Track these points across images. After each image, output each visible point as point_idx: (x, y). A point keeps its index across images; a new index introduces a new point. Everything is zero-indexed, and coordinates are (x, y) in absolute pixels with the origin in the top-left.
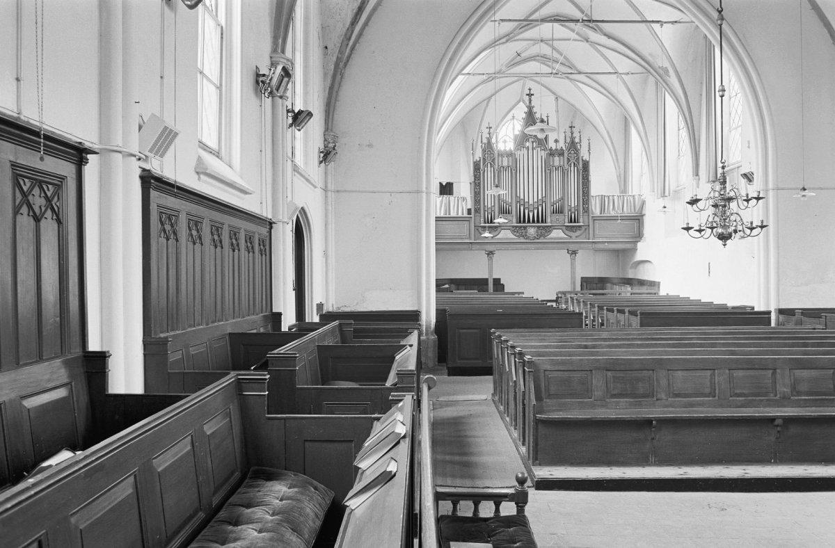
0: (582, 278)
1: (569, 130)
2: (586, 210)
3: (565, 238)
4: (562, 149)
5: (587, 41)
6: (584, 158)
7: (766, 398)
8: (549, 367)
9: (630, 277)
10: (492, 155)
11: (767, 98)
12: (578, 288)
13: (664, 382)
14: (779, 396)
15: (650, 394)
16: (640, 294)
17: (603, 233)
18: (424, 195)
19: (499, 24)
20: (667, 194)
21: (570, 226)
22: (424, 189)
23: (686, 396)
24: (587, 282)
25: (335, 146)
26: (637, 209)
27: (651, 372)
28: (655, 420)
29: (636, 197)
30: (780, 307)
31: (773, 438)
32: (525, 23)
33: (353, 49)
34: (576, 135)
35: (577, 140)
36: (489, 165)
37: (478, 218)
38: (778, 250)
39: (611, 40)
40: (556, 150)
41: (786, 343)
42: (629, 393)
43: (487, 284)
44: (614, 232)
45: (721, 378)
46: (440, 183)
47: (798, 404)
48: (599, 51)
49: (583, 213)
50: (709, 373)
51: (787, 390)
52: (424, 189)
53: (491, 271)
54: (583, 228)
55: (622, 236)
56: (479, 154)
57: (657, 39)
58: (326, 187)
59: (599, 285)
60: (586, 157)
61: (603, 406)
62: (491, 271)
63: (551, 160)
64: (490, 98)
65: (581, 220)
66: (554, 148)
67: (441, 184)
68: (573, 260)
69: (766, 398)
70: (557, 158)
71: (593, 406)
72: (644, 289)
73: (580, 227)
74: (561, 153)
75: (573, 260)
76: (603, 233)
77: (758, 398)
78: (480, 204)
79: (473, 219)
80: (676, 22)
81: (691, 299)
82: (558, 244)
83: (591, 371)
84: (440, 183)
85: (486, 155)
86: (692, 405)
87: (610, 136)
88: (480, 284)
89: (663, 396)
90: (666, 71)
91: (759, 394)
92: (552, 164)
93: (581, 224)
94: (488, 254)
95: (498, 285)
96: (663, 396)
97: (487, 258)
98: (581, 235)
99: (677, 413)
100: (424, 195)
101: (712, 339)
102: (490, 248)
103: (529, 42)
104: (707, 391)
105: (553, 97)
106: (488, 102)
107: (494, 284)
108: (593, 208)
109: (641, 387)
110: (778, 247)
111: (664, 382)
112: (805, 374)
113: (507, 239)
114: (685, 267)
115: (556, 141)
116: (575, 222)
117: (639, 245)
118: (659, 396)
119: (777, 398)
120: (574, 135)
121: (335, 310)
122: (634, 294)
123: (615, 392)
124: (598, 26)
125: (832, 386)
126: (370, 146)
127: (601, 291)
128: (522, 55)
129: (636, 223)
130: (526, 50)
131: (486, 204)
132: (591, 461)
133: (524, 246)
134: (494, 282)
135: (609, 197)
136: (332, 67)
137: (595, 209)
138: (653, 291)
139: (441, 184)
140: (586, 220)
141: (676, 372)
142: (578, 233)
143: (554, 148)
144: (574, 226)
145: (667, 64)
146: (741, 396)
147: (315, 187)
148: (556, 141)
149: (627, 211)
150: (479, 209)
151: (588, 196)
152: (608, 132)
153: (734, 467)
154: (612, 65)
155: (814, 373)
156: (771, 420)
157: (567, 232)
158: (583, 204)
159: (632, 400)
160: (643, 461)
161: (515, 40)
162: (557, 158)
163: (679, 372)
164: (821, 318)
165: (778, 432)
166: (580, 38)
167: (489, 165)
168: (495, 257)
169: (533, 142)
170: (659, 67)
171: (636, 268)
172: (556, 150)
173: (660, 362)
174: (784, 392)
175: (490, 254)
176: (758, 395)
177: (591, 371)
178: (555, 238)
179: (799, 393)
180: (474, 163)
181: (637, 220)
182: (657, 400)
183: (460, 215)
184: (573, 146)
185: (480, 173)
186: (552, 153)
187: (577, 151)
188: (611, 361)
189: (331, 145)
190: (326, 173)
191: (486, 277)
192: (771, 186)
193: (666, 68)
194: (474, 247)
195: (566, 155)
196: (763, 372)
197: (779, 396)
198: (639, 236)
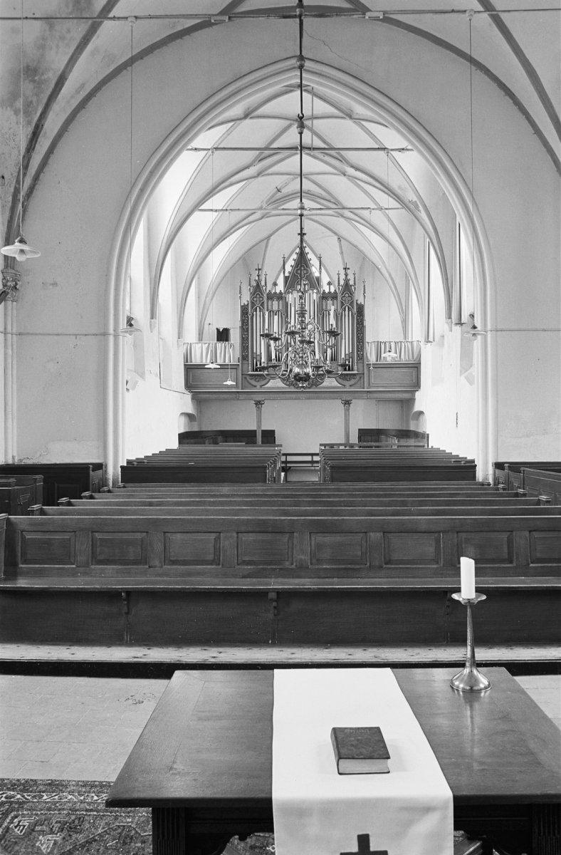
0: (359, 430)
1: (342, 272)
2: (361, 357)
3: (338, 387)
4: (281, 293)
5: (345, 175)
6: (359, 302)
7: (279, 567)
8: (27, 528)
9: (411, 429)
10: (261, 299)
11: (486, 236)
12: (354, 439)
13: (158, 547)
14: (295, 564)
15: (143, 560)
16: (407, 446)
17: (379, 381)
18: (111, 339)
19: (212, 152)
20: (431, 339)
21: (255, 375)
22: (111, 331)
23: (185, 563)
24: (364, 434)
25: (16, 284)
26: (415, 358)
27: (145, 534)
28: (124, 592)
29: (415, 344)
30: (499, 461)
31: (271, 616)
32: (267, 152)
33: (36, 178)
34: (351, 277)
35: (351, 282)
36: (258, 309)
37: (245, 366)
38: (497, 398)
39: (251, 168)
40: (330, 293)
41: (382, 501)
42: (117, 558)
43: (256, 436)
44: (391, 380)
45: (227, 543)
46: (217, 329)
47: (318, 574)
48: (359, 186)
49: (357, 360)
50: (213, 536)
51: (305, 558)
52: (111, 331)
53: (259, 421)
54: (358, 377)
55: (399, 385)
56: (246, 298)
57: (402, 172)
58: (5, 329)
59: (373, 438)
60: (361, 301)
61: (85, 574)
62: (259, 421)
63: (324, 304)
64: (268, 238)
65: (355, 367)
66: (327, 291)
67: (218, 330)
68: (347, 410)
69: (279, 567)
70: (275, 303)
71: (73, 574)
72: (412, 442)
73: (354, 375)
74: (334, 297)
75: (347, 410)
76: (379, 381)
77: (269, 567)
78: (248, 351)
79: (240, 365)
80: (403, 149)
81: (447, 452)
82: (332, 394)
83: (75, 532)
84: (217, 329)
85: (255, 299)
86: (190, 574)
87: (392, 279)
88: (247, 437)
89: (157, 563)
90: (417, 207)
91: (272, 563)
92: (324, 307)
93: (356, 372)
94: (256, 404)
95: (269, 436)
96: (157, 563)
97: (255, 409)
98: (355, 384)
99: (169, 583)
100: (111, 339)
101: (400, 495)
102: (259, 398)
103: (288, 176)
104: (210, 557)
105: (336, 237)
106: (267, 243)
107: (262, 437)
108: (368, 355)
109: (132, 553)
110: (496, 394)
111: (158, 547)
112: (328, 539)
113: (278, 388)
114: (458, 420)
115: (329, 284)
116: (349, 370)
117: (417, 394)
118: (151, 564)
119: (293, 566)
120: (349, 277)
121: (16, 462)
122: (400, 446)
123: (101, 557)
124: (342, 156)
125: (359, 553)
126: (55, 284)
127: (377, 444)
128: (283, 191)
129: (414, 371)
130: (286, 184)
131: (255, 351)
132: (57, 638)
133: (294, 396)
134: (262, 434)
135: (390, 342)
136: (10, 199)
137: (372, 357)
138: (421, 444)
139: (218, 330)
140: (361, 368)
141: (174, 535)
142: (352, 382)
143: (327, 291)
144: (347, 375)
145: (415, 199)
146: (251, 565)
147: (180, 336)
148: (329, 284)
149: (404, 358)
150: (247, 356)
151: (363, 342)
152: (390, 275)
153: (192, 649)
154: (376, 203)
155: (338, 538)
156: (261, 595)
157: (340, 381)
158: (358, 351)
159: (120, 567)
160: (116, 639)
161: (268, 174)
162: (275, 303)
163: (179, 536)
164: (520, 472)
165: (275, 607)
166: (335, 171)
167: (258, 309)
168: (264, 408)
169: (305, 285)
170: (410, 202)
171: (417, 420)
172: (330, 293)
173: (155, 522)
174: (301, 560)
175: (347, 403)
176: (270, 563)
177: (75, 532)
178: (273, 388)
179: (319, 561)
180: (242, 307)
181: (416, 367)
182: (150, 567)
183: (227, 362)
184: (347, 287)
185: (248, 317)
186: (324, 297)
187: (351, 294)
188: (469, 521)
189: (11, 284)
190: (5, 314)
191: (255, 429)
192: (489, 327)
193: (416, 201)
194: (242, 397)
195: (339, 298)
196: (278, 537)
197: (295, 564)
198: (417, 385)
